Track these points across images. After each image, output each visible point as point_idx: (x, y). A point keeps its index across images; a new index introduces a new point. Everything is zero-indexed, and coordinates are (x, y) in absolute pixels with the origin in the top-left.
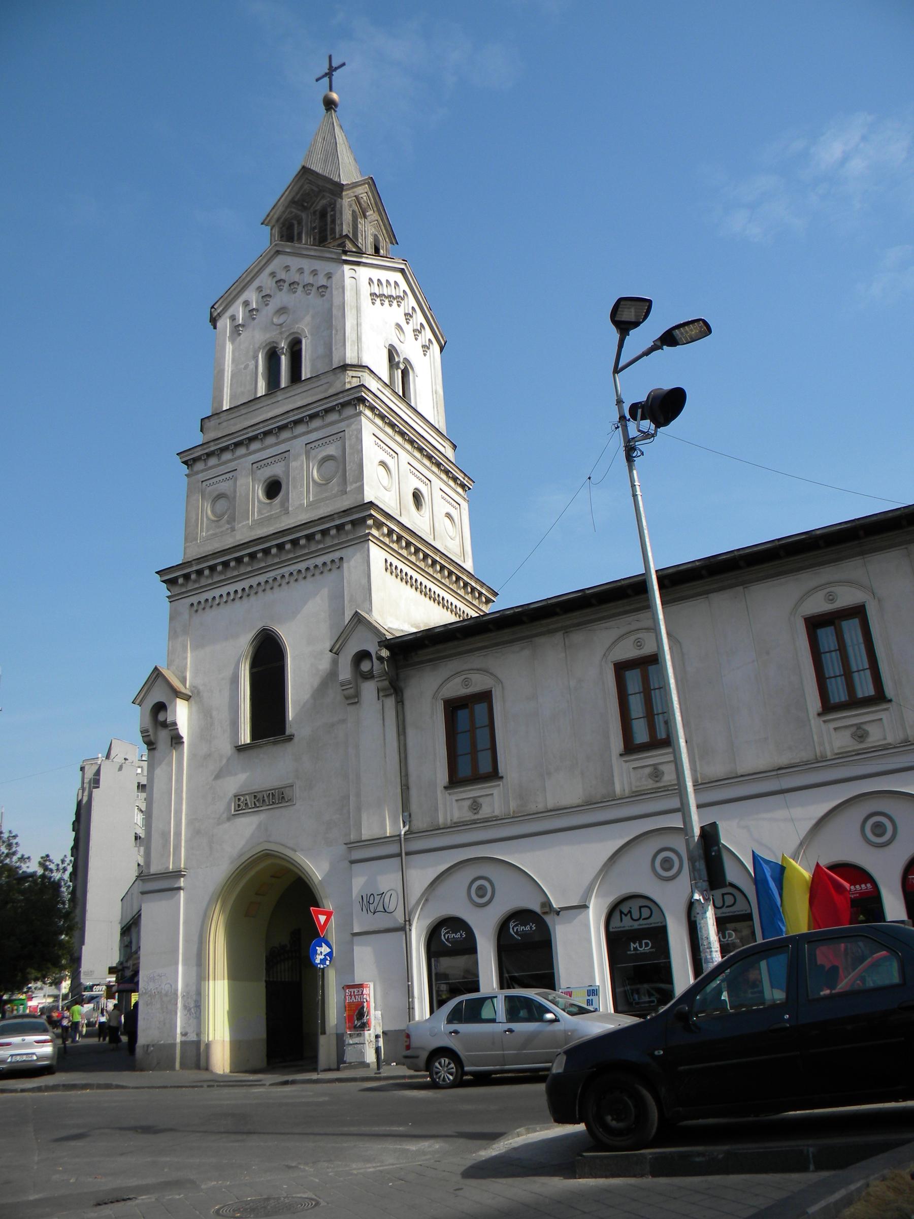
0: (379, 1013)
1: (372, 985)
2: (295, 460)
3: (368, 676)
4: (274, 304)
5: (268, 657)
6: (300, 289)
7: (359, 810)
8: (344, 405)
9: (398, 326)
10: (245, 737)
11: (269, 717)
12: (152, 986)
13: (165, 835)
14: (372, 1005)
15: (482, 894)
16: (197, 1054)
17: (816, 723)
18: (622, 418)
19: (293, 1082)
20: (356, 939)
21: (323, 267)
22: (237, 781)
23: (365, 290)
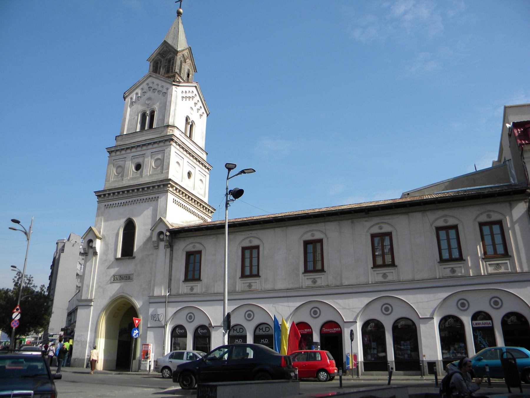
0: (153, 354)
1: (152, 345)
2: (147, 158)
3: (162, 240)
5: (130, 228)
6: (157, 92)
7: (154, 286)
8: (166, 140)
9: (191, 108)
10: (119, 255)
11: (128, 250)
12: (78, 338)
13: (88, 286)
14: (151, 351)
15: (190, 318)
16: (92, 363)
17: (301, 276)
18: (227, 194)
19: (122, 374)
20: (149, 329)
21: (166, 85)
22: (113, 271)
23: (180, 95)
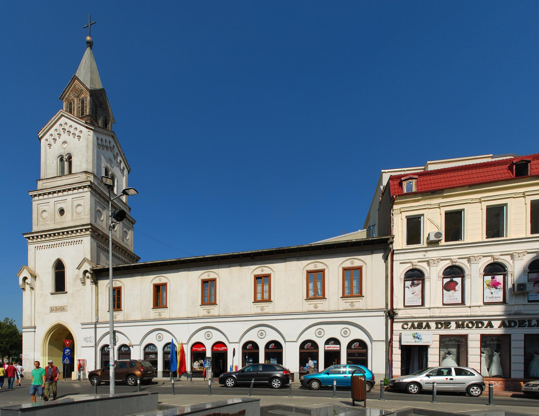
4: (59, 141)
